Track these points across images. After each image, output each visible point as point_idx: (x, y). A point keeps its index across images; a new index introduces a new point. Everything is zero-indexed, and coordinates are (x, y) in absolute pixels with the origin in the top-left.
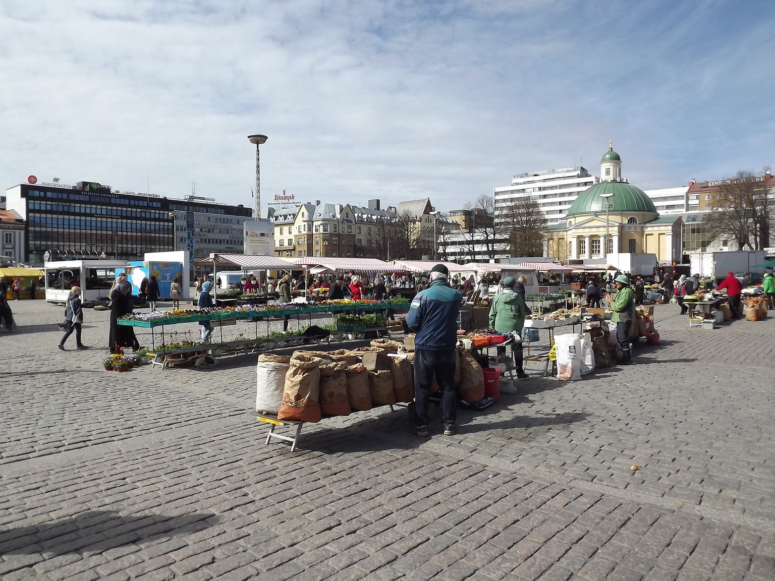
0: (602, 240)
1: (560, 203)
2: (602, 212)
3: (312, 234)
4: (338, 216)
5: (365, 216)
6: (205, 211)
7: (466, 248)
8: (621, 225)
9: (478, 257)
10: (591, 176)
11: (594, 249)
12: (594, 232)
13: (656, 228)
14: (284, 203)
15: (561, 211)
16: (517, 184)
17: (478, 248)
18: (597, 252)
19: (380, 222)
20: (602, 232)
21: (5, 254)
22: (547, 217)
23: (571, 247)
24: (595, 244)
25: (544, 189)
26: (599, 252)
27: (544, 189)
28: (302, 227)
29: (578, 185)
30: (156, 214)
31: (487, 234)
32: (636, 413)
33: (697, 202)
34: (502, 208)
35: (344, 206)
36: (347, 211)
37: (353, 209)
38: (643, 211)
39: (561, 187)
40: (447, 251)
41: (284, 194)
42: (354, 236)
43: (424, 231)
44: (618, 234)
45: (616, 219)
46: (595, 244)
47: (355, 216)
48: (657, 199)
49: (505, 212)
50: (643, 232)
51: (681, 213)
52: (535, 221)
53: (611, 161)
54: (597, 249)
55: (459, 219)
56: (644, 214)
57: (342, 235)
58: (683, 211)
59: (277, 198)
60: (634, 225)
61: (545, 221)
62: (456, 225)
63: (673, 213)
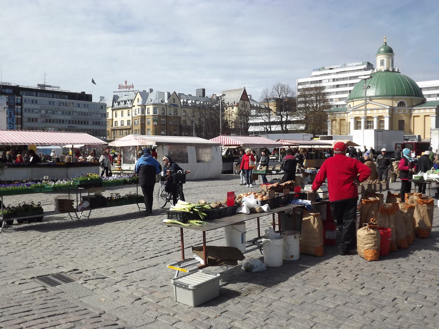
0: (375, 121)
2: (376, 97)
3: (145, 116)
4: (166, 101)
5: (189, 102)
6: (51, 96)
8: (392, 108)
13: (422, 111)
14: (126, 92)
16: (316, 76)
17: (274, 128)
20: (375, 114)
25: (337, 80)
27: (337, 80)
28: (137, 110)
30: (18, 100)
32: (353, 299)
35: (171, 93)
36: (174, 97)
38: (411, 96)
41: (126, 84)
42: (180, 118)
44: (435, 115)
45: (388, 103)
47: (180, 102)
48: (428, 89)
50: (411, 115)
53: (385, 54)
56: (412, 99)
57: (169, 117)
59: (120, 87)
60: (403, 108)
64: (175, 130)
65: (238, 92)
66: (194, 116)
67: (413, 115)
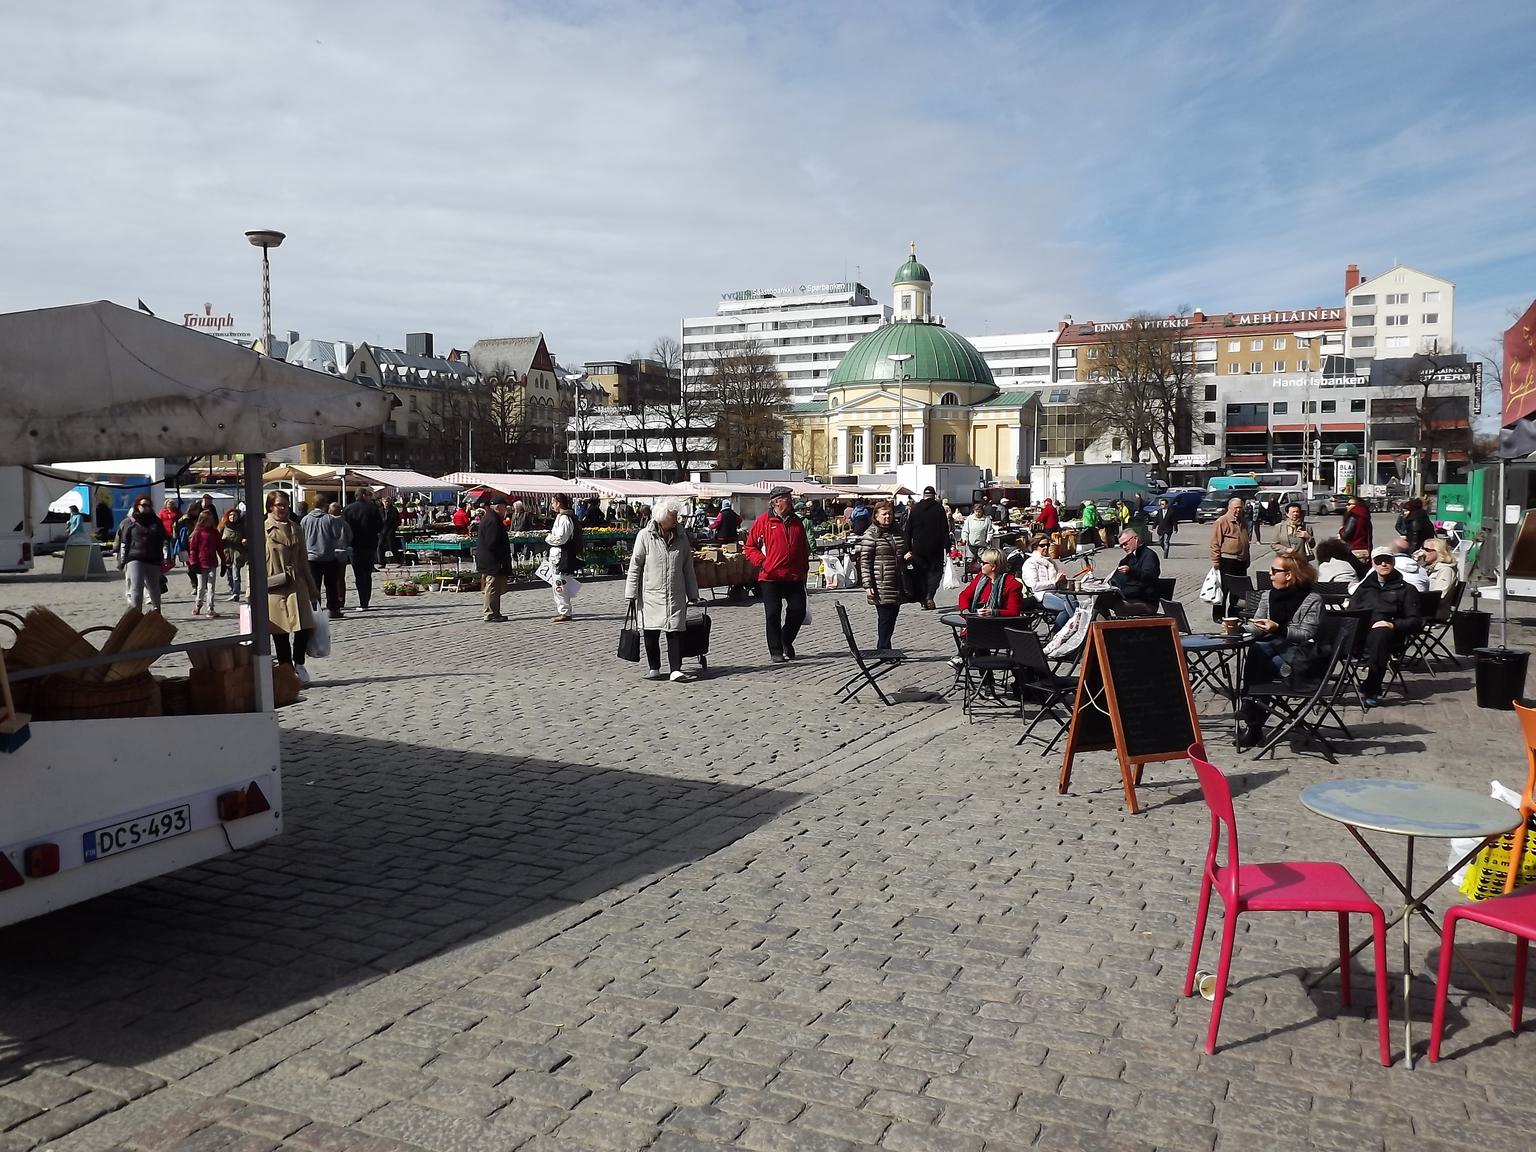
0: (894, 435)
1: (816, 357)
4: (343, 369)
5: (402, 371)
7: (629, 446)
9: (654, 465)
10: (875, 303)
11: (880, 453)
12: (879, 419)
13: (992, 415)
15: (816, 373)
17: (653, 446)
18: (885, 458)
19: (434, 385)
20: (892, 420)
21: (350, 488)
22: (790, 384)
23: (835, 448)
24: (880, 444)
25: (784, 325)
26: (888, 459)
27: (784, 325)
29: (851, 320)
31: (672, 418)
33: (1072, 362)
34: (703, 363)
35: (356, 346)
37: (376, 355)
38: (970, 381)
39: (817, 322)
40: (590, 451)
41: (208, 313)
43: (533, 405)
45: (920, 396)
46: (880, 444)
48: (998, 354)
49: (709, 371)
50: (968, 423)
51: (1041, 385)
52: (767, 393)
54: (886, 453)
55: (609, 382)
56: (970, 388)
58: (1048, 379)
61: (786, 392)
62: (599, 394)
63: (1027, 385)
64: (368, 448)
65: (525, 346)
66: (435, 413)
67: (974, 423)
